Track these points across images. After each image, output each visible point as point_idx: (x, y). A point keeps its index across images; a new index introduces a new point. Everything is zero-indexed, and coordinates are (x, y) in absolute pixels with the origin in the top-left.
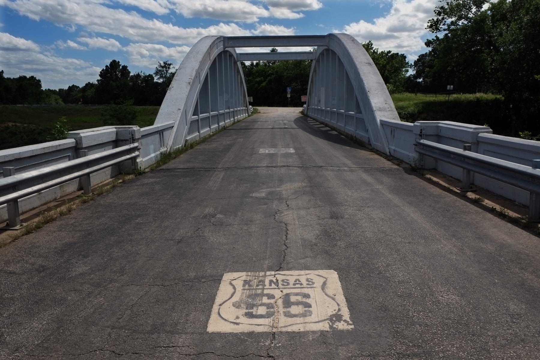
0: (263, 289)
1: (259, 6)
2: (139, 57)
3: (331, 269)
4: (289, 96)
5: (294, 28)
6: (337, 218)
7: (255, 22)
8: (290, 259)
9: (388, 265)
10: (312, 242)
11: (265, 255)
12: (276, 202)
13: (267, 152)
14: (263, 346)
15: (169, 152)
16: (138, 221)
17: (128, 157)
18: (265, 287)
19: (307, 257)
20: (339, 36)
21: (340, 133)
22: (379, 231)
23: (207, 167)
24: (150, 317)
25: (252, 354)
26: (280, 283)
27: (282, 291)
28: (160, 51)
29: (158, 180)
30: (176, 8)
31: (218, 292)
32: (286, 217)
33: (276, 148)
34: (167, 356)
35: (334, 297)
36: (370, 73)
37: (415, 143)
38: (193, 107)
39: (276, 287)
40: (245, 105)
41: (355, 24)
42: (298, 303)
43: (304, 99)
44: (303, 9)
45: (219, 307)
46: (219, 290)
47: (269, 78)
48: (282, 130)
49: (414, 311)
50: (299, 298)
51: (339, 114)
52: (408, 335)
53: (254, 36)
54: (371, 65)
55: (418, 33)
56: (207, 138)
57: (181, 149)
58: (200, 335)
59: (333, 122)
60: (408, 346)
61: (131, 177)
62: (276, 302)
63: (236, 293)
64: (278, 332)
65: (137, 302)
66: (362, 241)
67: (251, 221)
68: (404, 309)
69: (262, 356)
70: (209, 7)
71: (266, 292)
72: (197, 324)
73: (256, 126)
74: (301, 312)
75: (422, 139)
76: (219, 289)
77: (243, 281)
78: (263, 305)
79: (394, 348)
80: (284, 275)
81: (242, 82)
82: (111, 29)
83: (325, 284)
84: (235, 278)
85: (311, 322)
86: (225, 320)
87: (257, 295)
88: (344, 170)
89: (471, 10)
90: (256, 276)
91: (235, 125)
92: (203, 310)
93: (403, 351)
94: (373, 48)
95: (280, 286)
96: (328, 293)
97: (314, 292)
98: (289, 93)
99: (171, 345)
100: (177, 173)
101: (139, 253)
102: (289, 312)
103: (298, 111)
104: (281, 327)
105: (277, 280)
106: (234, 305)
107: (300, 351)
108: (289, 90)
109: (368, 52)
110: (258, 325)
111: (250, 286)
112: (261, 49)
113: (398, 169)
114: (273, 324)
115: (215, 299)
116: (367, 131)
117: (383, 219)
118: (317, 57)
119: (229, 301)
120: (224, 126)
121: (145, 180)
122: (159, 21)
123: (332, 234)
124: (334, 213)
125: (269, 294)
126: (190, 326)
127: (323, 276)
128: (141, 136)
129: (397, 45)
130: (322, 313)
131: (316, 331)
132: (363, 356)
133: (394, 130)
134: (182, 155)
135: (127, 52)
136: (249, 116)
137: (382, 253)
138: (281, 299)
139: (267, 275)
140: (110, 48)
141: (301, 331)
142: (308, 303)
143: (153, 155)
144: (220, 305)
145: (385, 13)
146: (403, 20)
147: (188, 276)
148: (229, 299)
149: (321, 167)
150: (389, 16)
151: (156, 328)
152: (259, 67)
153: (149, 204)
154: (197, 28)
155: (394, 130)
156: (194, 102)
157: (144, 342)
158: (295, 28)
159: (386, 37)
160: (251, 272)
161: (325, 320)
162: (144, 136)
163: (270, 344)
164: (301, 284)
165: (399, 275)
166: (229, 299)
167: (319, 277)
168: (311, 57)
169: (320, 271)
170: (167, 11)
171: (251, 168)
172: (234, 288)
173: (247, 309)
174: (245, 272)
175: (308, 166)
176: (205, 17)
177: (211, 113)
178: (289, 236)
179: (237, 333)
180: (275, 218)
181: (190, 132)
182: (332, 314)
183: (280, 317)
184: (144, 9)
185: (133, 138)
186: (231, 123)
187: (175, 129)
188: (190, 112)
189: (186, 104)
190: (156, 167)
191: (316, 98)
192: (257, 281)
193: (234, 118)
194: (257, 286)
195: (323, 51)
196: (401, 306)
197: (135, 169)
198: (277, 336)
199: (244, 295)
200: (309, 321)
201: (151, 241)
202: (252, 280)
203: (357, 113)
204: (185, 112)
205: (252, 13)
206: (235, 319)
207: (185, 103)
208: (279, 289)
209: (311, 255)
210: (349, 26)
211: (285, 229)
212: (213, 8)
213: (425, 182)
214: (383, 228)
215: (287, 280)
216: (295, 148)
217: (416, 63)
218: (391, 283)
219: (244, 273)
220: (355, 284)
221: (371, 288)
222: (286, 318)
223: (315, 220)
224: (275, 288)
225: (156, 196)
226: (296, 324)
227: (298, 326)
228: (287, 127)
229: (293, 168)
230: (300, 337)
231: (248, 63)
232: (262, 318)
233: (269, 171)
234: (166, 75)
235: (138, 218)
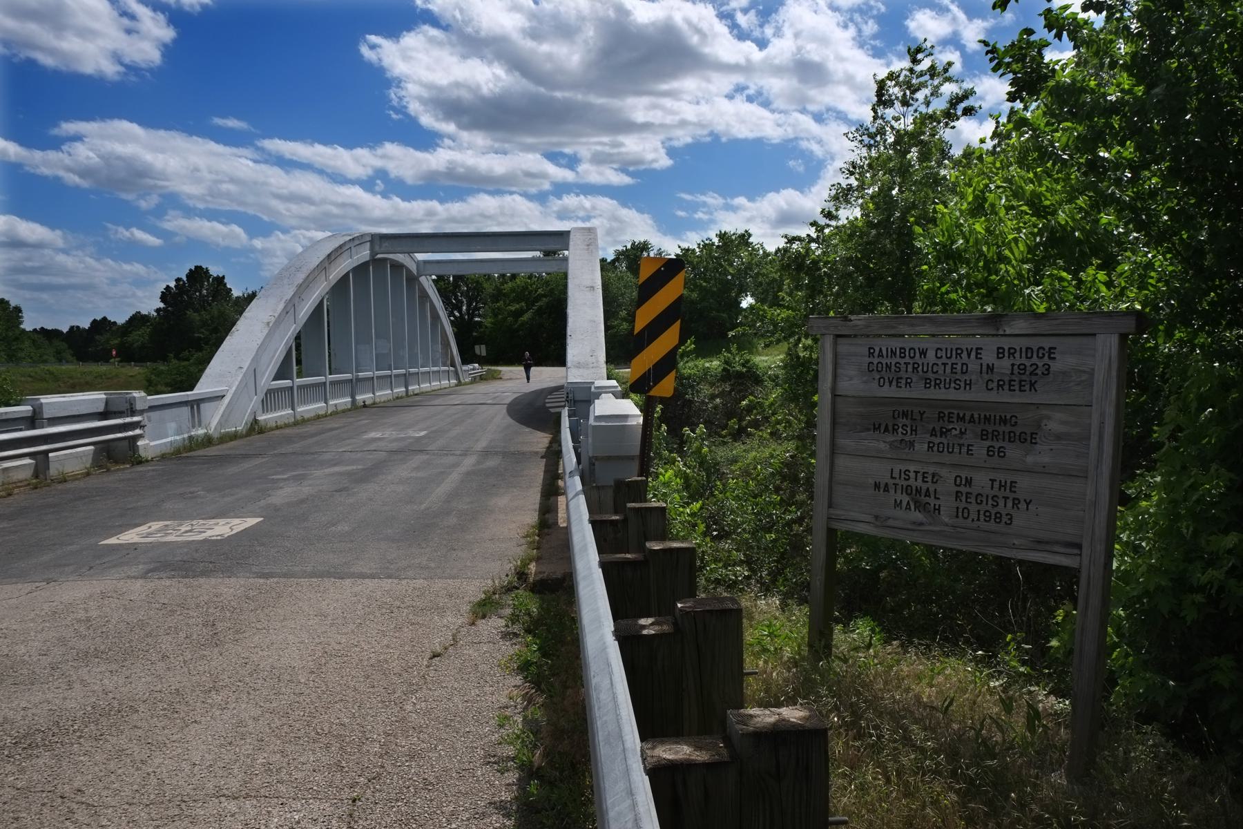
40: (449, 362)
156: (279, 356)
162: (152, 408)
187: (226, 400)
188: (268, 373)
189: (256, 359)
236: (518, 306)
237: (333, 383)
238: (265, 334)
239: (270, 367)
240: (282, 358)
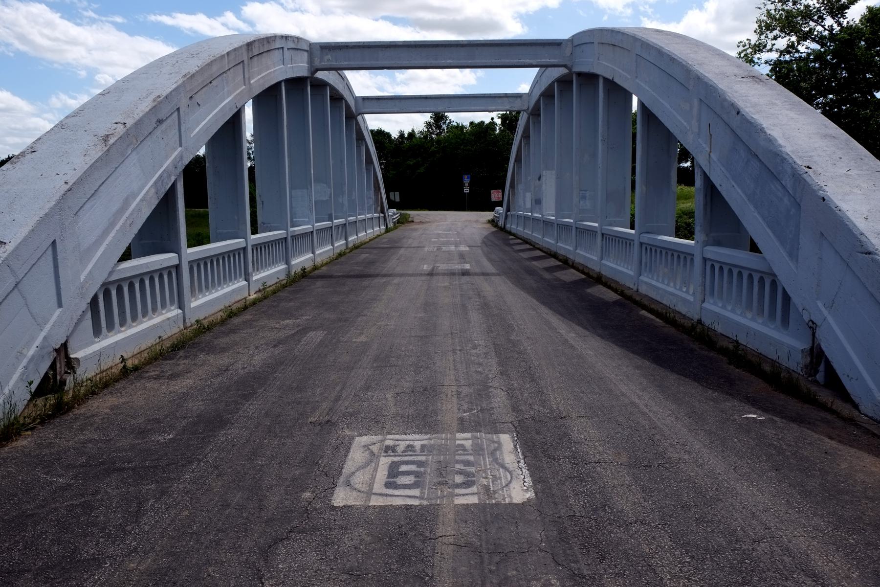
4: (467, 190)
36: (773, 104)
40: (379, 209)
89: (822, 22)
98: (467, 185)
108: (467, 181)
136: (388, 230)
152: (414, 140)
156: (138, 209)
228: (467, 266)
237: (258, 247)
238: (90, 160)
239: (112, 235)
240: (146, 212)
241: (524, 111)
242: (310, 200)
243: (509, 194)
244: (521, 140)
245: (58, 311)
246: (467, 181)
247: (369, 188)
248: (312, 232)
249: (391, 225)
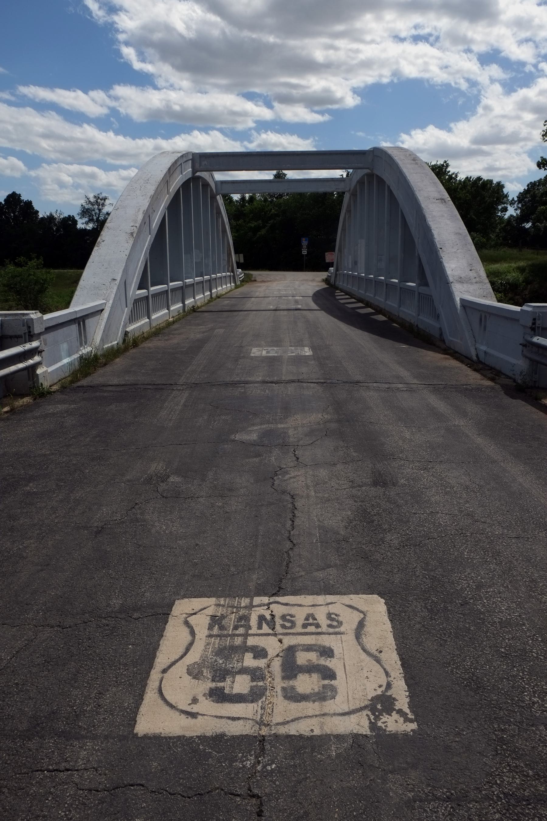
0: (246, 636)
1: (257, 101)
2: (56, 187)
3: (373, 594)
4: (305, 252)
5: (314, 139)
6: (385, 484)
7: (250, 129)
8: (298, 569)
9: (479, 587)
10: (339, 534)
11: (252, 560)
12: (276, 452)
13: (264, 353)
14: (241, 768)
15: (96, 355)
16: (28, 488)
17: (21, 366)
18: (250, 632)
19: (329, 566)
20: (390, 152)
21: (392, 318)
22: (462, 512)
23: (159, 382)
24: (30, 698)
25: (218, 788)
26: (278, 621)
27: (280, 641)
28: (93, 176)
29: (73, 406)
30: (120, 106)
31: (161, 642)
32: (294, 482)
33: (279, 347)
34: (52, 794)
35: (378, 655)
36: (443, 216)
37: (522, 341)
38: (139, 274)
39: (271, 631)
40: (230, 269)
41: (419, 131)
42: (310, 669)
43: (329, 257)
44: (330, 107)
45: (160, 675)
46: (164, 638)
47: (272, 221)
48: (292, 312)
49: (534, 692)
50: (312, 656)
51: (389, 286)
52: (523, 750)
53: (249, 151)
54: (445, 202)
55: (522, 147)
56: (164, 328)
57: (115, 347)
58: (120, 741)
59: (380, 300)
60: (524, 775)
61: (27, 400)
62: (269, 666)
63: (195, 643)
64: (270, 736)
65: (9, 665)
66: (431, 532)
67: (230, 490)
68: (513, 687)
69: (238, 795)
70: (175, 104)
71: (251, 641)
72: (118, 715)
73: (249, 305)
74: (316, 690)
75: (535, 335)
76: (164, 634)
77: (209, 618)
78: (244, 671)
79: (498, 782)
80: (286, 604)
81: (224, 231)
82: (12, 141)
83: (361, 625)
84: (194, 611)
85: (335, 714)
86: (171, 706)
87: (234, 649)
88: (398, 389)
90: (233, 607)
91: (211, 304)
92: (130, 683)
93: (516, 788)
94: (449, 172)
95: (278, 629)
96: (368, 647)
97: (342, 643)
98: (305, 247)
99: (63, 765)
100: (105, 394)
101: (25, 555)
102: (293, 688)
103: (320, 279)
104: (278, 724)
105: (273, 616)
106: (189, 672)
107: (312, 784)
108: (305, 243)
109: (439, 178)
110: (234, 719)
111: (222, 628)
112: (261, 173)
113: (493, 388)
114: (261, 718)
115: (154, 657)
116: (438, 317)
117: (467, 487)
118: (352, 188)
119: (181, 661)
120: (193, 307)
121: (51, 407)
122: (92, 127)
123: (375, 517)
124: (380, 474)
125: (257, 647)
126: (104, 719)
127: (358, 607)
128: (44, 330)
129: (486, 166)
130: (356, 692)
131: (343, 735)
132: (437, 798)
133: (485, 316)
134: (117, 360)
135: (37, 179)
136: (237, 287)
137: (468, 559)
138: (279, 658)
139: (254, 604)
140: (8, 172)
141: (314, 734)
142: (330, 670)
143: (66, 361)
144: (164, 671)
145: (469, 113)
146: (497, 125)
147: (108, 605)
148: (182, 657)
149: (358, 382)
150: (474, 117)
151: (38, 724)
152: (255, 203)
153: (53, 454)
154: (155, 138)
155: (485, 316)
157: (12, 757)
158: (317, 138)
159: (469, 154)
160: (225, 597)
161: (361, 709)
162: (49, 329)
163: (254, 766)
164: (318, 626)
165: (500, 608)
166: (182, 657)
167: (350, 610)
168: (341, 187)
169: (352, 596)
170: (105, 111)
171: (235, 384)
172: (193, 633)
173: (213, 681)
174: (214, 597)
175: (334, 381)
176: (167, 120)
177: (171, 284)
178: (297, 522)
179: (192, 737)
180: (273, 484)
181: (132, 319)
182: (374, 694)
183: (274, 700)
184: (67, 107)
185: (30, 332)
186: (206, 300)
187: (106, 314)
189: (125, 271)
190: (72, 382)
191: (350, 257)
192: (235, 616)
193: (211, 291)
194: (236, 628)
195: (364, 175)
196: (508, 679)
197: (34, 387)
198: (268, 747)
199: (210, 649)
200: (332, 712)
201: (47, 531)
202: (227, 615)
203: (419, 285)
204: (125, 284)
205: (245, 114)
206: (189, 704)
207: (124, 269)
208: (275, 635)
209: (338, 562)
210: (409, 134)
211: (290, 506)
212: (181, 106)
213: (541, 413)
214: (467, 505)
215: (292, 616)
216: (313, 348)
217: (522, 197)
218: (486, 626)
219: (213, 601)
220: (417, 626)
221: (449, 636)
222: (286, 702)
223: (345, 489)
224: (268, 635)
225: (66, 439)
226: (305, 717)
227: (308, 721)
228: (300, 307)
229: (309, 384)
230: (313, 750)
231: (236, 197)
232: (240, 702)
233: (267, 391)
234: (98, 217)
235: (30, 482)
236: (256, 223)
241: (347, 191)
242: (192, 262)
243: (338, 257)
244: (346, 213)
245: (126, 309)
246: (305, 243)
247: (223, 253)
248: (193, 284)
249: (238, 283)
